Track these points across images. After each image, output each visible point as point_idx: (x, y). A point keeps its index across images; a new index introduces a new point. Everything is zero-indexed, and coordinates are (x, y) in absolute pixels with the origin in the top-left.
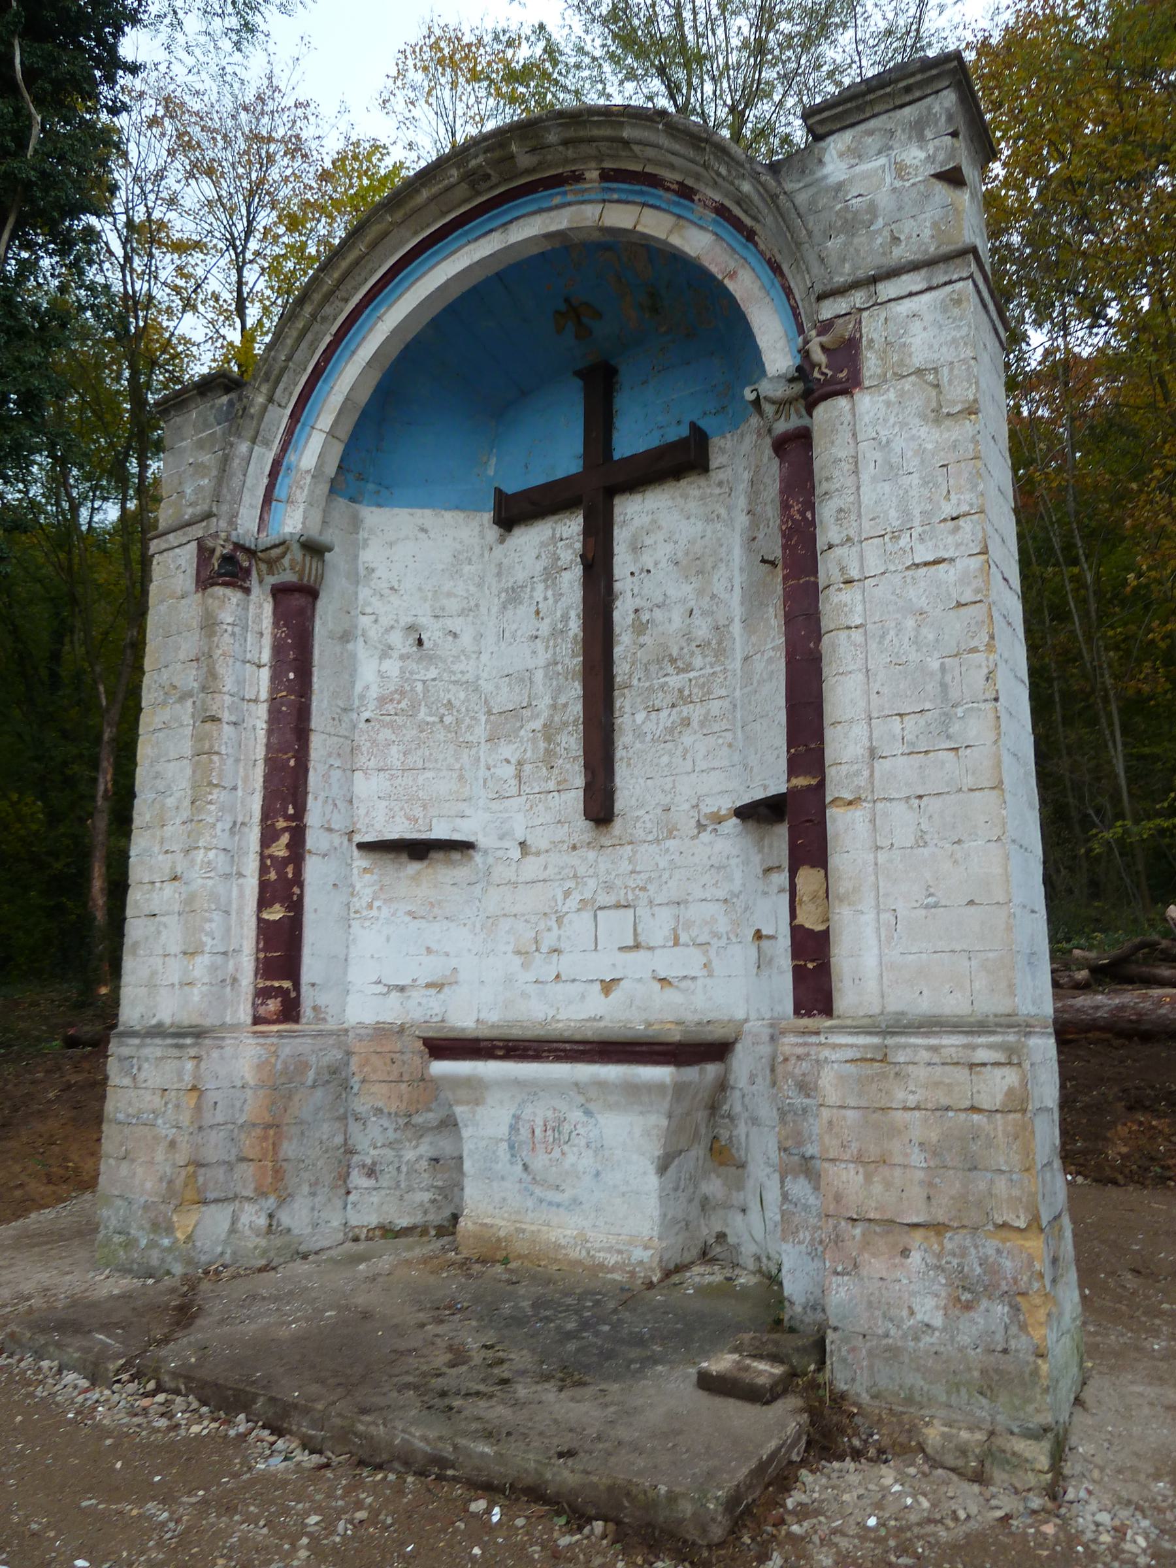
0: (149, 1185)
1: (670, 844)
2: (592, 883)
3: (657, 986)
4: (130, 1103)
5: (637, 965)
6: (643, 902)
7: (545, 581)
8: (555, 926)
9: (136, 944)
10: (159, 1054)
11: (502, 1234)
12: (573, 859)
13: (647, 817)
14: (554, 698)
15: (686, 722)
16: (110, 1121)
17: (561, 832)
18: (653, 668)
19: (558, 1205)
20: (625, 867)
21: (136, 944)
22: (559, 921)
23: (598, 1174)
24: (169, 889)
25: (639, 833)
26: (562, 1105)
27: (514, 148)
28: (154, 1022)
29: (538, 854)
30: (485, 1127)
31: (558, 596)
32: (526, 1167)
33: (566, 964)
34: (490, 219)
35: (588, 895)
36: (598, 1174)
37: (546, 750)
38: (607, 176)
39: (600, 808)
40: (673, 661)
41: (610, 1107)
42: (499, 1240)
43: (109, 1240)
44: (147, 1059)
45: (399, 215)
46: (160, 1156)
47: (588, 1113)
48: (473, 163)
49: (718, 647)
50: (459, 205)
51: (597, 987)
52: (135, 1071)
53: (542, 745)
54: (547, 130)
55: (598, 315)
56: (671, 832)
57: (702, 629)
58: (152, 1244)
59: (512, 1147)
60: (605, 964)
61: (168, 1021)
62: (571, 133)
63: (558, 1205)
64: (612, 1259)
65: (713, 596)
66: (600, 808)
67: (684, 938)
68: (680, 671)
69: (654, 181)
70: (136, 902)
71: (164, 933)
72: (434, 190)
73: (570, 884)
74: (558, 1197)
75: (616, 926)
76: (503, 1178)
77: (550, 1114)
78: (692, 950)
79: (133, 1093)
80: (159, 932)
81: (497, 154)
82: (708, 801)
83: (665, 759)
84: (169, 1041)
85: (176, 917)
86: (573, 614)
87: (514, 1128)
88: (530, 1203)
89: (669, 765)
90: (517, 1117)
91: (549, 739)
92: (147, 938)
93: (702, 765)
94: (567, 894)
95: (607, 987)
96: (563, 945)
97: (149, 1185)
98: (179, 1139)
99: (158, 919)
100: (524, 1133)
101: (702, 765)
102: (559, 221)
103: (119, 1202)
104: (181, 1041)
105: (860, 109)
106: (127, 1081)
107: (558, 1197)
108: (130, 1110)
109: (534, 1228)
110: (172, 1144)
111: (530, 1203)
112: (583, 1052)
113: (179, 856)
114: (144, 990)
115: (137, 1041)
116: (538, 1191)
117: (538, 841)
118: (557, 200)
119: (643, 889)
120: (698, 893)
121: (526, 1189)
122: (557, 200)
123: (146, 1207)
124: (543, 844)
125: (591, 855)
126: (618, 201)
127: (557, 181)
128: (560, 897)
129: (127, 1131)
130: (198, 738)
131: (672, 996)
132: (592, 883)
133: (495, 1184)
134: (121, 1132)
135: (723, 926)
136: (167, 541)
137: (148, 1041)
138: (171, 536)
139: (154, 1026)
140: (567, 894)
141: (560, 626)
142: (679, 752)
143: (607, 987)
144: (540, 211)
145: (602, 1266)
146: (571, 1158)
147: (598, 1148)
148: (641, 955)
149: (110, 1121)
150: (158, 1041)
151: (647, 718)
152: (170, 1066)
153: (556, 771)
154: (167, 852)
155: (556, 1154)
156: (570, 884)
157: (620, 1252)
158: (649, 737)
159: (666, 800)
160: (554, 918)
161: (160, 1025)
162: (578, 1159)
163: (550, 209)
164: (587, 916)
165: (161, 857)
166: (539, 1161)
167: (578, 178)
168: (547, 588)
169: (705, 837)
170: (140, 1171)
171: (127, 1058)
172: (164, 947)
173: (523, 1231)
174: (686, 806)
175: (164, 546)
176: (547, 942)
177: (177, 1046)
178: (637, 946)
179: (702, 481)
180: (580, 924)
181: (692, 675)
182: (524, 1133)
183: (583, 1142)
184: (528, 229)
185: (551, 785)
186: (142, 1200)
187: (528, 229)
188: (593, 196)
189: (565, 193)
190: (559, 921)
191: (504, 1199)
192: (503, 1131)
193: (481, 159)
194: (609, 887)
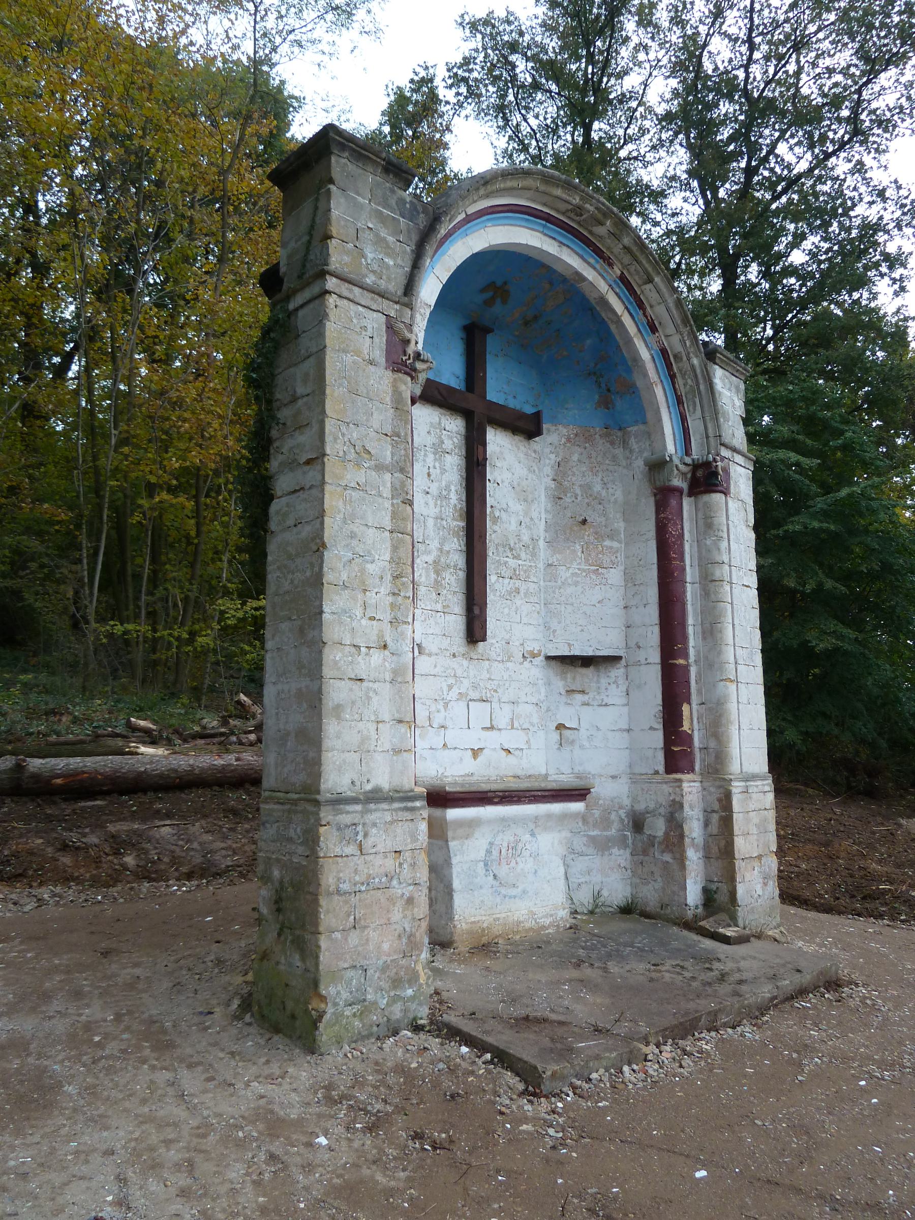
0: (386, 946)
1: (509, 664)
2: (466, 683)
3: (504, 753)
4: (356, 871)
5: (492, 740)
6: (495, 700)
7: (435, 454)
8: (442, 710)
9: (338, 708)
10: (389, 818)
11: (485, 925)
12: (454, 663)
13: (497, 645)
14: (442, 544)
15: (518, 591)
16: (329, 894)
17: (445, 643)
18: (501, 549)
19: (515, 897)
20: (485, 675)
21: (338, 708)
22: (446, 705)
23: (536, 872)
24: (377, 657)
25: (493, 655)
26: (519, 831)
27: (608, 223)
28: (369, 787)
29: (430, 655)
30: (466, 855)
31: (443, 471)
32: (495, 876)
33: (452, 736)
34: (559, 233)
35: (463, 690)
36: (536, 872)
37: (436, 580)
38: (623, 278)
39: (475, 630)
40: (511, 549)
41: (546, 829)
42: (483, 930)
43: (338, 1016)
44: (374, 825)
45: (542, 188)
46: (396, 915)
47: (533, 835)
48: (587, 206)
49: (532, 548)
50: (552, 208)
51: (470, 753)
52: (360, 838)
53: (433, 576)
54: (628, 235)
55: (504, 302)
56: (510, 658)
57: (526, 538)
58: (394, 1000)
59: (486, 865)
60: (475, 738)
61: (386, 786)
62: (634, 249)
63: (515, 897)
64: (547, 921)
65: (532, 519)
66: (475, 630)
67: (516, 725)
68: (515, 557)
69: (641, 305)
70: (336, 663)
71: (375, 699)
72: (564, 196)
73: (451, 681)
74: (513, 892)
75: (479, 712)
76: (481, 887)
77: (512, 839)
78: (520, 732)
79: (359, 861)
80: (369, 698)
81: (600, 216)
82: (529, 643)
83: (506, 611)
84: (396, 805)
85: (388, 685)
86: (453, 488)
87: (489, 852)
88: (498, 900)
89: (508, 614)
90: (491, 844)
91: (437, 573)
92: (353, 703)
93: (525, 620)
94: (450, 687)
95: (476, 753)
96: (449, 723)
97: (386, 946)
98: (416, 895)
99: (365, 684)
100: (495, 853)
101: (525, 620)
102: (590, 274)
103: (351, 973)
104: (410, 804)
105: (727, 364)
106: (351, 849)
107: (513, 892)
108: (357, 878)
109: (504, 915)
110: (410, 901)
111: (498, 900)
112: (544, 797)
113: (387, 628)
114: (356, 757)
115: (359, 807)
116: (503, 891)
117: (431, 645)
118: (592, 261)
119: (496, 691)
120: (524, 699)
121: (496, 891)
122: (592, 261)
123: (385, 968)
124: (434, 649)
125: (465, 663)
126: (617, 294)
127: (598, 253)
128: (445, 689)
129: (353, 900)
130: (394, 515)
131: (511, 759)
132: (466, 683)
133: (476, 893)
134: (346, 902)
135: (535, 720)
136: (351, 291)
137: (372, 806)
138: (357, 290)
139: (371, 792)
140: (450, 687)
141: (444, 493)
142: (514, 608)
143: (476, 753)
144: (582, 257)
145: (544, 928)
146: (521, 865)
147: (535, 856)
148: (494, 733)
149: (329, 894)
150: (384, 806)
151: (497, 581)
152: (401, 829)
153: (442, 598)
154: (372, 619)
155: (513, 864)
156: (451, 681)
157: (551, 916)
158: (498, 594)
159: (507, 637)
160: (441, 703)
161: (377, 790)
162: (526, 865)
163: (588, 263)
164: (463, 704)
165: (364, 622)
166: (503, 871)
167: (611, 265)
168: (435, 459)
169: (527, 664)
170: (373, 934)
171: (347, 826)
172: (376, 713)
173: (498, 919)
174: (517, 643)
175: (345, 293)
176: (437, 720)
177: (406, 809)
178: (492, 728)
179: (525, 443)
180: (459, 708)
181: (520, 562)
182: (495, 853)
183: (528, 853)
184: (571, 259)
185: (439, 607)
186: (380, 962)
187: (571, 259)
188: (608, 278)
189: (598, 262)
190: (446, 705)
191: (482, 901)
192: (482, 854)
193: (591, 208)
194: (475, 687)
